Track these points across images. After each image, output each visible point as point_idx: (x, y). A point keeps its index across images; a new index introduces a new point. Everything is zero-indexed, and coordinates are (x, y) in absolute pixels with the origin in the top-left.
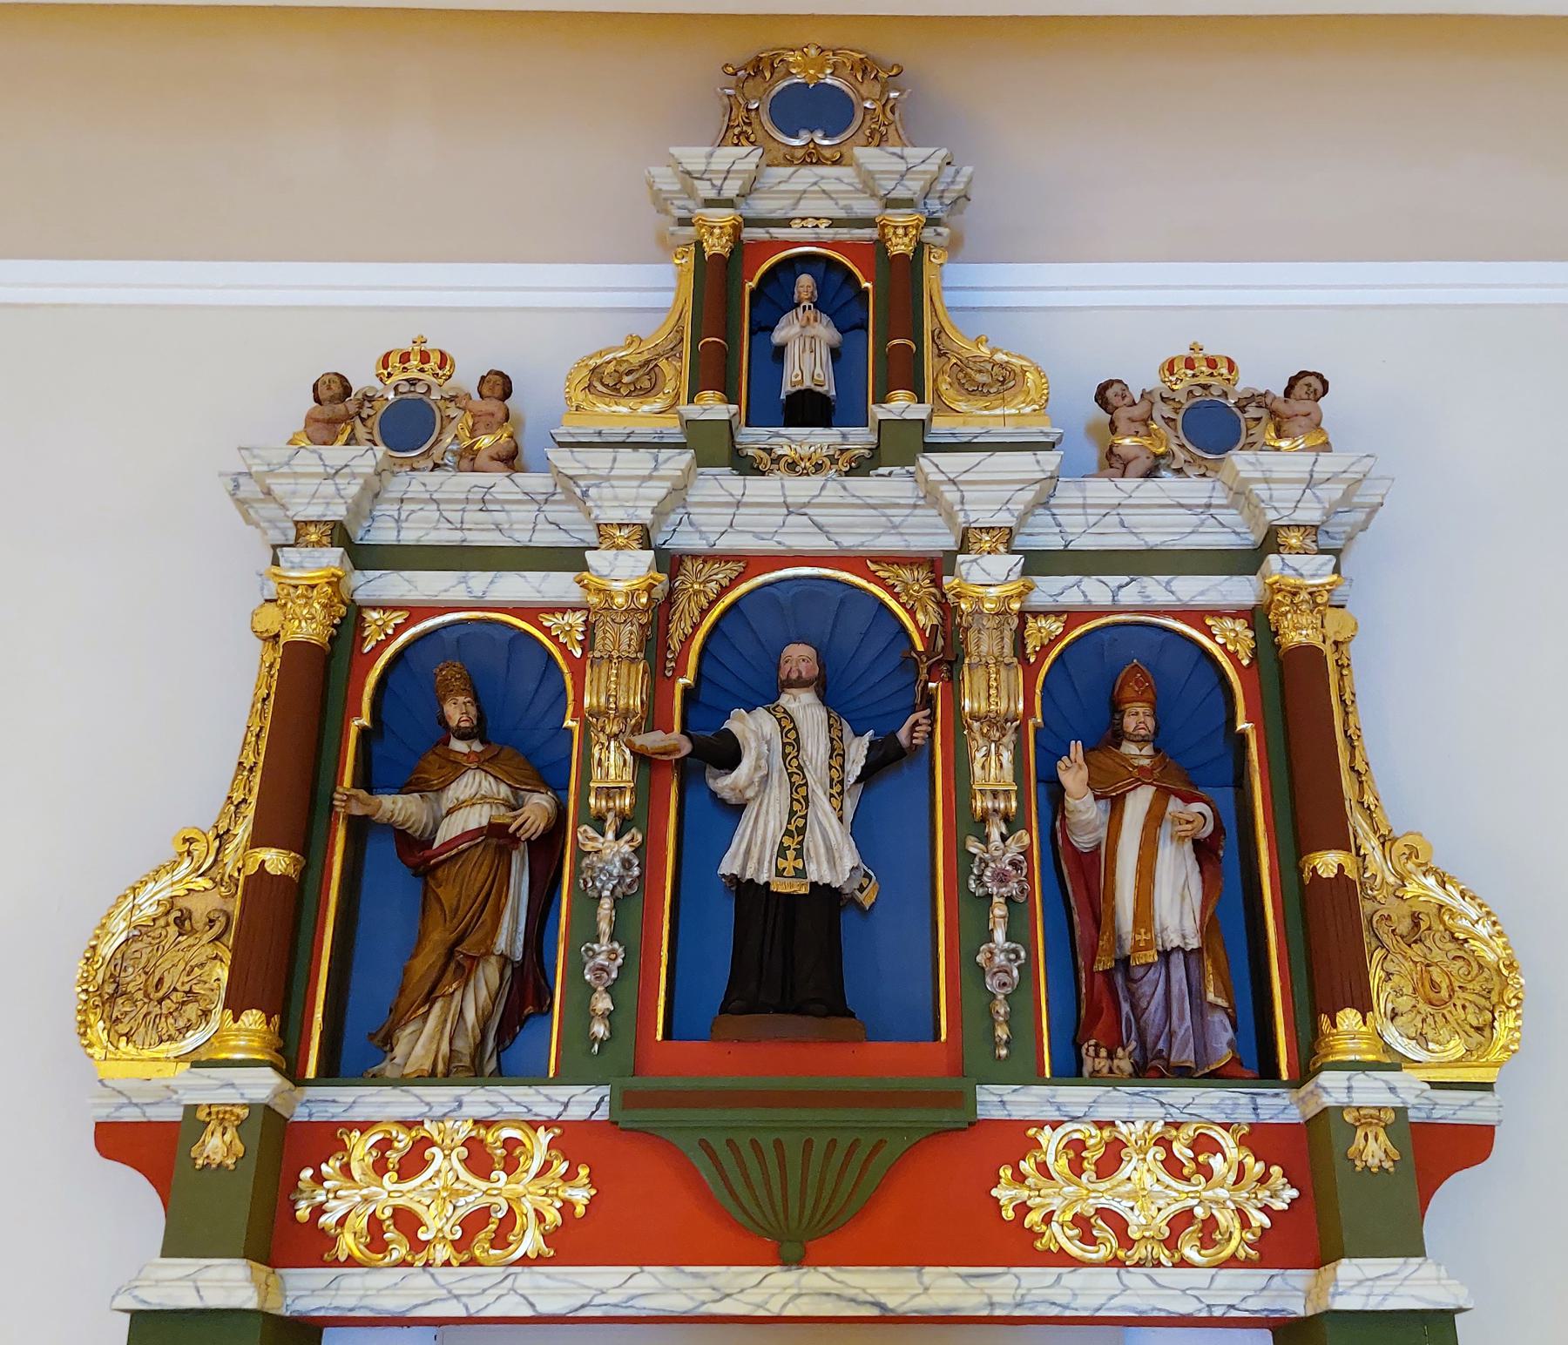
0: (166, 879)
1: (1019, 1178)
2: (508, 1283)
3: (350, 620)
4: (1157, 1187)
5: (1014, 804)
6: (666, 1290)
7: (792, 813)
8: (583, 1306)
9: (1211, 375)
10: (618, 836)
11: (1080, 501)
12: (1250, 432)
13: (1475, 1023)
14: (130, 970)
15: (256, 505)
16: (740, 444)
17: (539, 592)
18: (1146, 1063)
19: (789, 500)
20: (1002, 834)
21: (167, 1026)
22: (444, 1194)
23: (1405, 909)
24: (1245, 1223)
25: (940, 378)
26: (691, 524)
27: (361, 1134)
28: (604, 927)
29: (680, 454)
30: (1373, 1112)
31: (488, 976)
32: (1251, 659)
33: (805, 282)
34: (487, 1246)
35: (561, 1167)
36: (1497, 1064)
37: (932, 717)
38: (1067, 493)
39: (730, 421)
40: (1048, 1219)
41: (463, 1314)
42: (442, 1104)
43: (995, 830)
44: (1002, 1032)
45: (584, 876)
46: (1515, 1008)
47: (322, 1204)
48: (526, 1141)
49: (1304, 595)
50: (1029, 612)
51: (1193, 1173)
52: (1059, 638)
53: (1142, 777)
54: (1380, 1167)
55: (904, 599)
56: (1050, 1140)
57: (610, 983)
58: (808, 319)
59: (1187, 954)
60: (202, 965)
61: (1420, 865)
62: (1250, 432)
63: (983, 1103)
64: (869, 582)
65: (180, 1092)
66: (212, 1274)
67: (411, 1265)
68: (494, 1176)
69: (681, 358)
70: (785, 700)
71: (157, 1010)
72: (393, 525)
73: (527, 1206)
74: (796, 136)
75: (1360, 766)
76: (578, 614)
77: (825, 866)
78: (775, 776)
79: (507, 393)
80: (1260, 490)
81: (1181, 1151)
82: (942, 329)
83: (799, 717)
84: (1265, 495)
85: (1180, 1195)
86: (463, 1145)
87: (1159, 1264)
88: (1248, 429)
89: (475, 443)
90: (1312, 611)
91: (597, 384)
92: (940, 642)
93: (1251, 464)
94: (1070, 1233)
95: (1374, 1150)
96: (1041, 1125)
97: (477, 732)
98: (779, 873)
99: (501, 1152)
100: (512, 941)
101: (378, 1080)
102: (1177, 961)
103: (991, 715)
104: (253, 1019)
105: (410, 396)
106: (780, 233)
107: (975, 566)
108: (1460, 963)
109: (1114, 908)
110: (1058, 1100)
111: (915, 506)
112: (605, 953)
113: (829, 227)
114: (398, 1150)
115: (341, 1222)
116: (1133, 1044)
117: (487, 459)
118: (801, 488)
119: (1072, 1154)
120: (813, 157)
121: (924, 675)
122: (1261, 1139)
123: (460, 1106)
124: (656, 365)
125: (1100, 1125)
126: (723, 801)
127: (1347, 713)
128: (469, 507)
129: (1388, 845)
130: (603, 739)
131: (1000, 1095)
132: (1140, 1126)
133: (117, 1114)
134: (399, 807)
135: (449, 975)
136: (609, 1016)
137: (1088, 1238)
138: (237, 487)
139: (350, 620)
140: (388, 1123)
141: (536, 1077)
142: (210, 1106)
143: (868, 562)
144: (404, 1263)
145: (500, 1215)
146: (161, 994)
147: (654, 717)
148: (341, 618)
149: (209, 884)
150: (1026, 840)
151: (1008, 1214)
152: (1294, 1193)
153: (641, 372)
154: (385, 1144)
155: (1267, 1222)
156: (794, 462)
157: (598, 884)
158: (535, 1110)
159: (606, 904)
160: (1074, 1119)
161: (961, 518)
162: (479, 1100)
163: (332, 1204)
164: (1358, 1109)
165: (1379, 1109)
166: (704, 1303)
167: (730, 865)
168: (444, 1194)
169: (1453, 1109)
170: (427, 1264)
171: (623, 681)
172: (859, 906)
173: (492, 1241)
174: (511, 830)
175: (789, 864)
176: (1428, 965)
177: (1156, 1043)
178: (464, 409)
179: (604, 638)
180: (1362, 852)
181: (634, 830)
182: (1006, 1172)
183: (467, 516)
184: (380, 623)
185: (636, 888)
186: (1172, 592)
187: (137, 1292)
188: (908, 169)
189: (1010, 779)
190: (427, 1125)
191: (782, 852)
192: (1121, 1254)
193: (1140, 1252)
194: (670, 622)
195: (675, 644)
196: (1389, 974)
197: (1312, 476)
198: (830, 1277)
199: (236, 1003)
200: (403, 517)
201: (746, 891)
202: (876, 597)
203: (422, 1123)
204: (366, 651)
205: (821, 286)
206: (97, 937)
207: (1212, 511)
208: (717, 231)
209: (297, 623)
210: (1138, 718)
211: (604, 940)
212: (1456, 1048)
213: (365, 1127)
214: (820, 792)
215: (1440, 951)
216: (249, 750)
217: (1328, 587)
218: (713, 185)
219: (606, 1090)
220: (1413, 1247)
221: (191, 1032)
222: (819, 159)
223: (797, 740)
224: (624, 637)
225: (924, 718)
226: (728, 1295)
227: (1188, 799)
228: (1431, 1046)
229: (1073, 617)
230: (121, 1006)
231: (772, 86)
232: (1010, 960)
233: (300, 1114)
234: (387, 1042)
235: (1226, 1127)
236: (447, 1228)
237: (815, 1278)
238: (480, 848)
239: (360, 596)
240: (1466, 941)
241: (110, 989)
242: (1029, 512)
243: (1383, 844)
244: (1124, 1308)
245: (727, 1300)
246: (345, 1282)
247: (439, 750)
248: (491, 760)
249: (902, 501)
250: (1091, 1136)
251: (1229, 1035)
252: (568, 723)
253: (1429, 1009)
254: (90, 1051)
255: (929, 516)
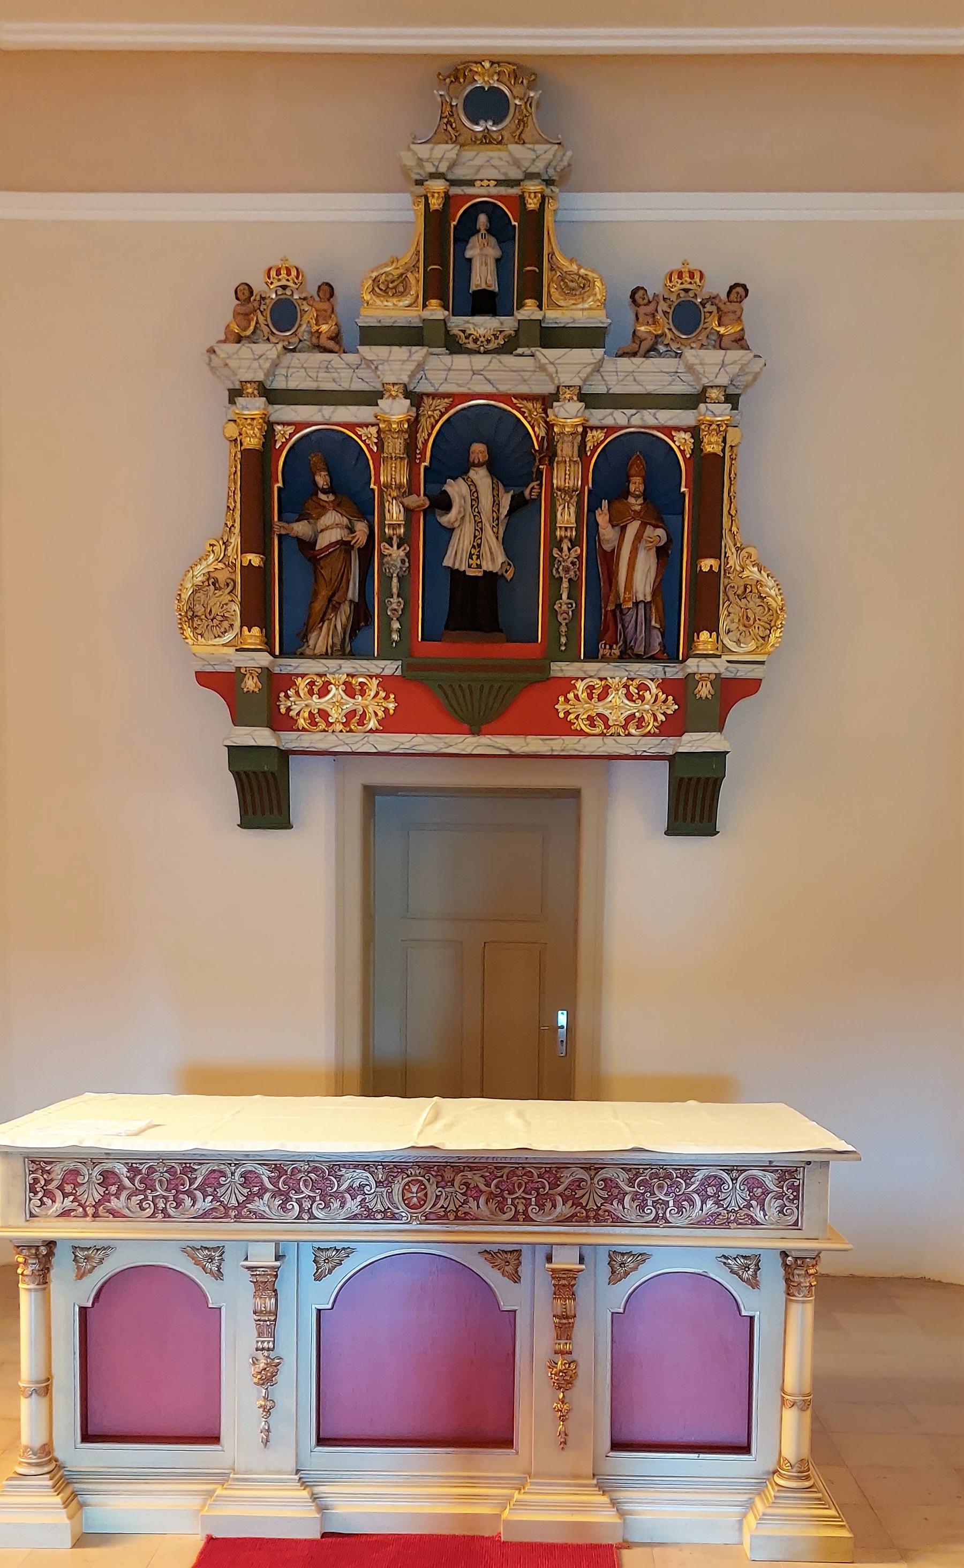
0: (204, 563)
1: (567, 701)
2: (366, 739)
3: (269, 434)
4: (622, 704)
5: (574, 533)
6: (428, 743)
7: (475, 536)
8: (396, 749)
9: (691, 283)
10: (399, 548)
11: (615, 370)
12: (706, 321)
13: (761, 635)
14: (197, 606)
15: (220, 369)
16: (450, 327)
17: (356, 417)
18: (626, 651)
19: (474, 368)
20: (568, 547)
21: (217, 631)
22: (337, 704)
23: (742, 583)
24: (656, 719)
25: (551, 284)
26: (426, 379)
27: (302, 679)
28: (395, 590)
29: (421, 349)
30: (707, 675)
31: (346, 609)
32: (691, 455)
33: (482, 219)
34: (356, 725)
35: (382, 694)
36: (769, 654)
37: (541, 485)
38: (609, 365)
39: (444, 320)
40: (577, 718)
41: (350, 750)
42: (333, 667)
43: (565, 545)
44: (563, 640)
45: (385, 566)
46: (780, 628)
47: (290, 706)
48: (368, 683)
49: (714, 426)
50: (588, 427)
51: (637, 699)
52: (602, 442)
53: (636, 515)
54: (706, 697)
55: (529, 419)
56: (580, 685)
57: (398, 616)
58: (484, 244)
59: (645, 604)
60: (226, 604)
61: (752, 562)
62: (706, 321)
63: (553, 670)
64: (513, 409)
65: (233, 661)
66: (257, 733)
67: (327, 731)
68: (356, 697)
69: (418, 271)
70: (472, 473)
71: (211, 624)
72: (284, 378)
73: (371, 710)
74: (477, 124)
75: (733, 512)
76: (374, 428)
77: (490, 563)
78: (467, 516)
79: (332, 294)
80: (699, 368)
81: (633, 690)
82: (553, 254)
83: (478, 483)
84: (701, 371)
85: (631, 708)
86: (343, 684)
87: (620, 735)
88: (705, 319)
89: (319, 329)
90: (717, 434)
91: (377, 289)
92: (546, 444)
93: (695, 356)
94: (585, 723)
95: (705, 690)
96: (577, 679)
97: (330, 490)
98: (470, 566)
99: (358, 687)
100: (353, 594)
101: (302, 656)
102: (641, 606)
103: (566, 489)
104: (256, 630)
105: (283, 297)
106: (469, 190)
107: (562, 409)
108: (761, 607)
109: (617, 582)
110: (585, 669)
111: (535, 371)
112: (395, 602)
113: (496, 186)
114: (317, 686)
115: (298, 714)
116: (621, 643)
117: (326, 340)
118: (480, 361)
119: (589, 691)
120: (486, 139)
121: (537, 463)
122: (666, 685)
123: (341, 668)
124: (406, 276)
125: (601, 679)
126: (445, 527)
127: (731, 484)
128: (320, 370)
129: (739, 552)
130: (390, 499)
131: (561, 667)
132: (617, 679)
133: (203, 668)
134: (301, 529)
135: (330, 611)
136: (399, 631)
137: (593, 725)
138: (210, 360)
139: (269, 434)
140: (312, 674)
141: (369, 656)
142: (246, 667)
143: (513, 399)
144: (324, 731)
145: (360, 713)
146: (212, 617)
147: (412, 488)
148: (266, 432)
149: (223, 566)
150: (579, 551)
151: (561, 715)
152: (676, 707)
153: (399, 281)
154: (312, 683)
155: (664, 719)
156: (476, 338)
157: (391, 571)
158: (372, 670)
159: (395, 580)
160: (591, 677)
161: (556, 382)
162: (348, 666)
163: (294, 707)
164: (701, 674)
165: (709, 674)
166: (442, 748)
167: (447, 562)
168: (337, 704)
169: (744, 672)
170: (333, 731)
171: (398, 471)
172: (506, 579)
173: (358, 723)
174: (352, 543)
175: (474, 562)
176: (747, 609)
177: (630, 643)
178: (312, 306)
179: (388, 446)
180: (727, 556)
181: (406, 545)
182: (561, 699)
183: (320, 375)
184: (282, 432)
185: (407, 572)
186: (656, 419)
187: (232, 739)
188: (537, 157)
189: (573, 520)
190: (328, 675)
191: (471, 556)
192: (605, 731)
193: (612, 730)
194: (417, 433)
195: (420, 445)
196: (729, 613)
197: (723, 362)
198: (490, 739)
199: (247, 622)
200: (289, 375)
201: (456, 575)
202: (517, 417)
203: (326, 675)
204: (277, 448)
205: (490, 220)
206: (181, 590)
207: (679, 374)
208: (436, 195)
209: (248, 439)
210: (636, 485)
211: (395, 596)
212: (752, 645)
213: (303, 676)
214: (488, 525)
215: (754, 602)
216: (231, 500)
217: (726, 422)
218: (434, 165)
219: (400, 663)
220: (720, 729)
221: (227, 634)
222: (490, 140)
223: (477, 497)
224: (395, 445)
225: (537, 485)
226: (451, 746)
227: (656, 527)
228: (742, 645)
229: (609, 430)
230: (197, 622)
231: (465, 88)
232: (569, 608)
233: (277, 670)
234: (305, 637)
235: (652, 680)
236: (340, 718)
237: (485, 740)
238: (338, 551)
239: (272, 419)
240: (765, 597)
241: (190, 613)
242: (591, 374)
243: (737, 551)
244: (603, 752)
245: (451, 747)
246: (303, 737)
247: (314, 498)
248: (339, 505)
249: (528, 369)
250: (597, 684)
251: (660, 639)
252: (372, 486)
253: (744, 629)
254: (187, 641)
255: (542, 376)
